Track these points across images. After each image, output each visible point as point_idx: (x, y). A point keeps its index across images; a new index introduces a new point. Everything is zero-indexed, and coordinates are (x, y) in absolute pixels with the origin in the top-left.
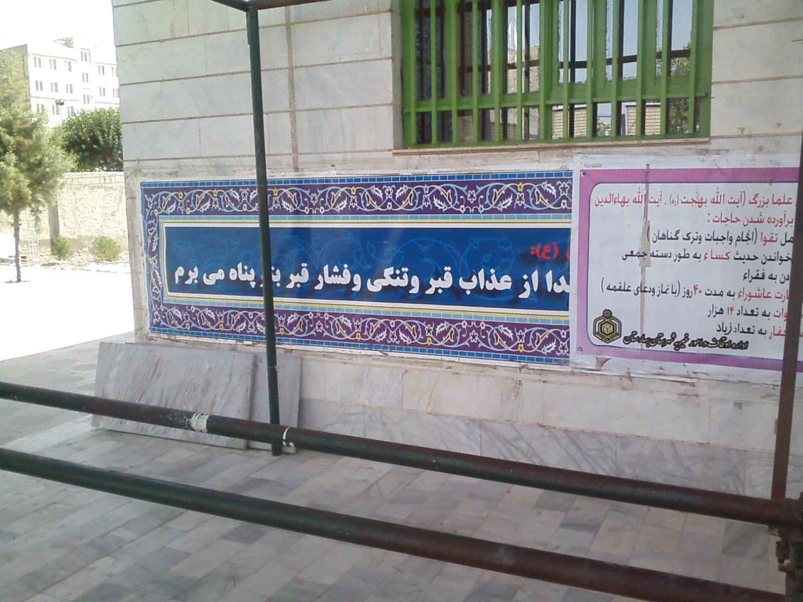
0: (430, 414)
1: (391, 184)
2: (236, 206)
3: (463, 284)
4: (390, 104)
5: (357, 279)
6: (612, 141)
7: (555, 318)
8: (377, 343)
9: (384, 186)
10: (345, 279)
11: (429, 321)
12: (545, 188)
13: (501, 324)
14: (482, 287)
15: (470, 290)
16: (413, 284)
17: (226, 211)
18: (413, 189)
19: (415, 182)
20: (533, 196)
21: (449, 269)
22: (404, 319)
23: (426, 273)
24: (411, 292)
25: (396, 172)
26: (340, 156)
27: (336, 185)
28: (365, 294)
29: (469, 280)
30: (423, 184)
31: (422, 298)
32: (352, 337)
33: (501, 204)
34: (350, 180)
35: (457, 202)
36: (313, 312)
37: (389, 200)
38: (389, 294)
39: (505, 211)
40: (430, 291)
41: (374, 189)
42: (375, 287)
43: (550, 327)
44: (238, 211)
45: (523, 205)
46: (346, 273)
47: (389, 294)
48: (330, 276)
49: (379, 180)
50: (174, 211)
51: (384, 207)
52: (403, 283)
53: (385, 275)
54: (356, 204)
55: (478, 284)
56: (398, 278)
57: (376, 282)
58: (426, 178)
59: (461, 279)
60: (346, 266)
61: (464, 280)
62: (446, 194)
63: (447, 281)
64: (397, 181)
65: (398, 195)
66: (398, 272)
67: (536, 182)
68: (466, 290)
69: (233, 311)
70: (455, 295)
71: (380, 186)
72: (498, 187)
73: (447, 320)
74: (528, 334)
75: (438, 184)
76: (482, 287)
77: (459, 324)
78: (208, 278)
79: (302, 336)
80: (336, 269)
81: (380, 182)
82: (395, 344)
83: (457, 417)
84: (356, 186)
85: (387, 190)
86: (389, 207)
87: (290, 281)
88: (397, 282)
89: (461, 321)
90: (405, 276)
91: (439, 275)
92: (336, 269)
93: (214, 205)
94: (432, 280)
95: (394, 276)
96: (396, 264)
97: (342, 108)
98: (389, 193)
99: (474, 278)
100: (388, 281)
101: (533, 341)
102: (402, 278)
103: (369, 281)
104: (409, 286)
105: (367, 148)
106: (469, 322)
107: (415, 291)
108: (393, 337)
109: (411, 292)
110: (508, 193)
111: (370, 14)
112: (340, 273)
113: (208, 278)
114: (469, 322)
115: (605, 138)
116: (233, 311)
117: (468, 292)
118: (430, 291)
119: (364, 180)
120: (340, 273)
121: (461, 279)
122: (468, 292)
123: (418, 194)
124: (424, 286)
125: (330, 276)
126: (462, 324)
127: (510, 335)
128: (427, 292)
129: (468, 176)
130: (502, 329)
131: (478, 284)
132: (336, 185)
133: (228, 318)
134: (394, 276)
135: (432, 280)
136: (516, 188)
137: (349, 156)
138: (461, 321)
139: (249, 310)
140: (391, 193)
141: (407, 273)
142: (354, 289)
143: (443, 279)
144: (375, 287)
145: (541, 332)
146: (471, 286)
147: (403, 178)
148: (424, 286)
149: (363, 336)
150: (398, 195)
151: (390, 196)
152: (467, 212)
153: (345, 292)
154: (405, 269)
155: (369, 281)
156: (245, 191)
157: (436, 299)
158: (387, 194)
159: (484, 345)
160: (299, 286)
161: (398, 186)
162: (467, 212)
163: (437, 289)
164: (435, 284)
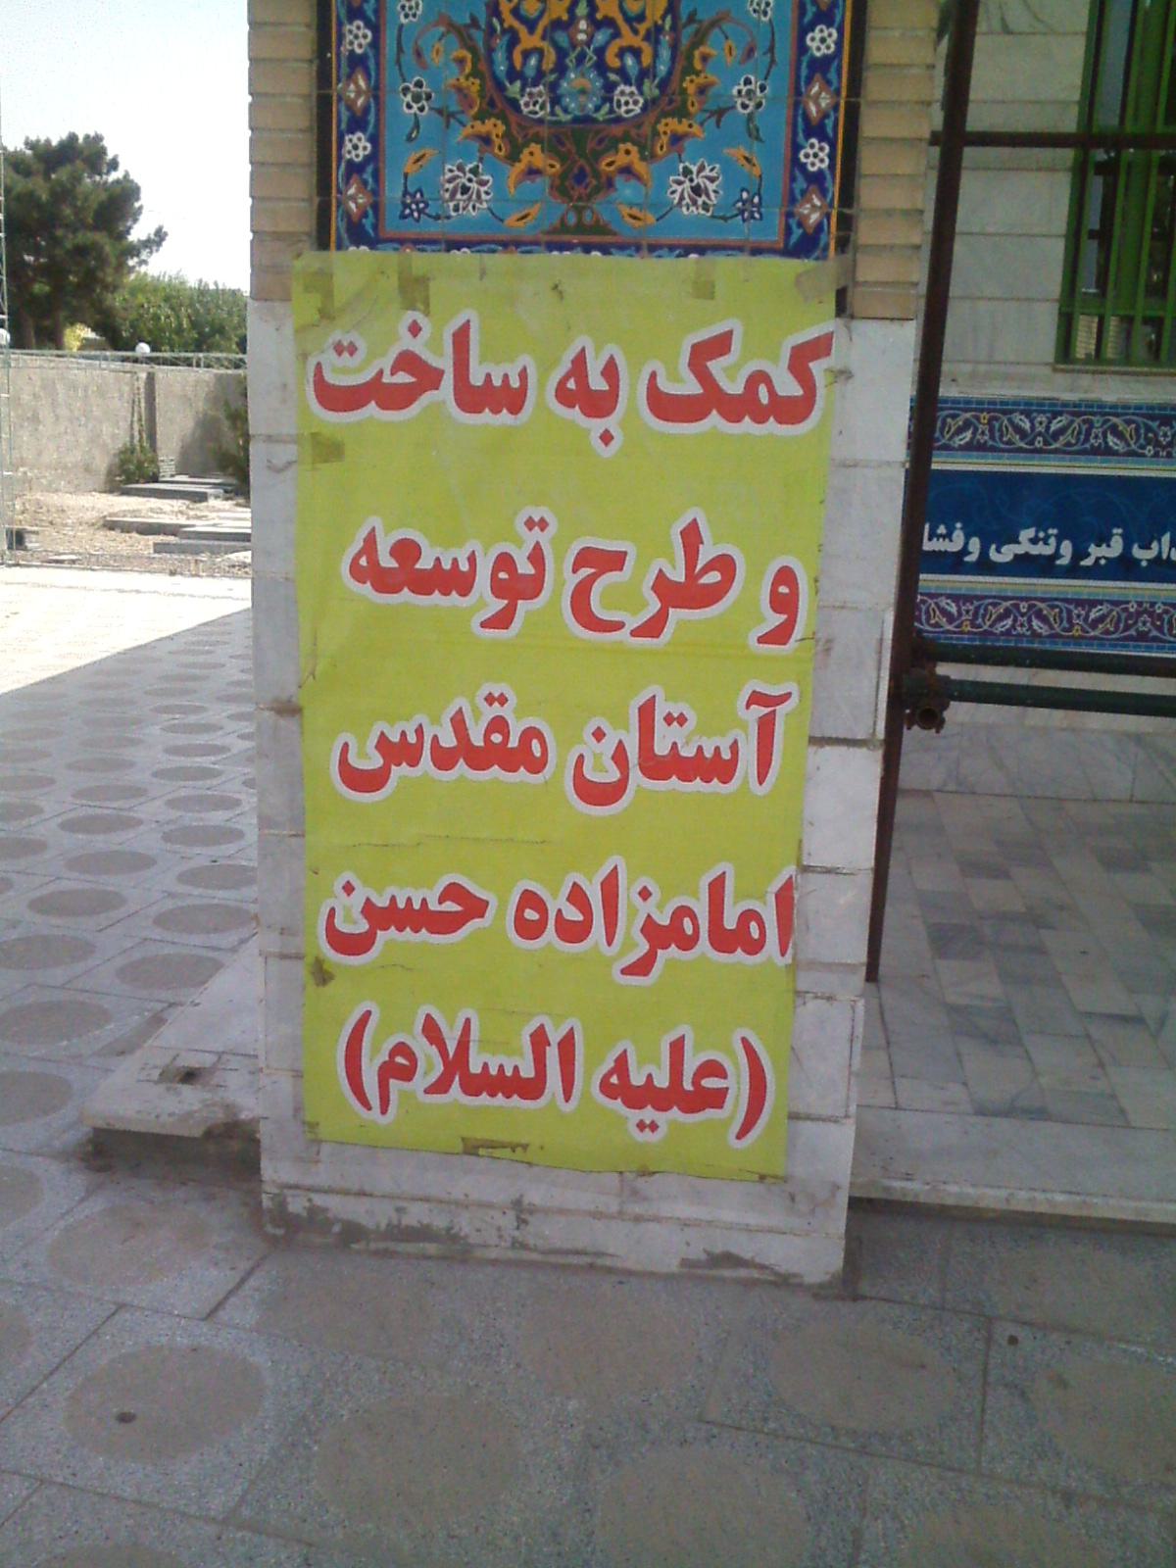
0: (1063, 730)
1: (1044, 412)
2: (1022, 439)
3: (1137, 552)
4: (1053, 300)
5: (975, 544)
6: (1119, 365)
7: (970, 585)
8: (995, 634)
9: (1035, 414)
10: (955, 545)
11: (1079, 603)
12: (1017, 420)
13: (941, 595)
14: (1165, 556)
15: (1148, 561)
16: (971, 548)
17: (1002, 446)
18: (1078, 420)
19: (1076, 410)
20: (1000, 430)
21: (1120, 531)
22: (1043, 600)
23: (1082, 537)
24: (1058, 562)
25: (1055, 395)
26: (967, 368)
27: (959, 409)
28: (985, 566)
29: (1146, 546)
30: (1094, 414)
31: (1074, 571)
32: (956, 627)
33: (957, 439)
34: (980, 402)
35: (1142, 441)
36: (1136, 602)
37: (1040, 434)
38: (1025, 565)
39: (962, 448)
40: (1088, 562)
41: (1018, 418)
42: (1005, 555)
43: (1006, 599)
44: (1028, 447)
45: (986, 442)
46: (959, 536)
47: (1025, 565)
48: (930, 539)
49: (1026, 404)
50: (967, 443)
51: (1031, 443)
52: (1048, 550)
53: (1020, 539)
54: (986, 438)
55: (1160, 553)
56: (1041, 543)
57: (1004, 549)
58: (1100, 407)
59: (1136, 546)
60: (959, 525)
61: (1141, 547)
62: (1128, 430)
63: (1115, 548)
64: (1055, 409)
65: (1053, 427)
66: (1041, 535)
67: (1005, 412)
68: (1141, 560)
69: (991, 601)
70: (1124, 568)
71: (1028, 414)
72: (954, 417)
73: (1107, 601)
74: (977, 609)
75: (1117, 415)
76: (1165, 556)
77: (1124, 606)
78: (998, 551)
79: (1114, 636)
80: (942, 530)
81: (1029, 408)
82: (1023, 635)
83: (1105, 732)
84: (989, 411)
85: (1039, 419)
86: (1039, 443)
87: (1088, 555)
88: (1035, 550)
89: (1128, 602)
90: (1052, 541)
91: (1104, 539)
92: (942, 530)
93: (978, 437)
94: (1093, 545)
95: (1034, 541)
96: (1041, 525)
97: (979, 298)
98: (1041, 423)
99: (1155, 545)
100: (1024, 547)
101: (984, 616)
102: (1046, 543)
103: (993, 547)
104: (1057, 555)
105: (1012, 358)
106: (1140, 604)
107: (1064, 561)
108: (1022, 625)
109: (1058, 562)
110: (967, 425)
111: (1040, 169)
112: (948, 536)
113: (998, 551)
114: (1140, 604)
115: (1111, 362)
116: (991, 601)
117: (1144, 564)
118: (1088, 562)
119: (1002, 403)
120: (948, 536)
121: (1136, 546)
122: (1144, 564)
123: (1084, 427)
124: (1080, 553)
125: (930, 539)
126: (1130, 606)
127: (954, 609)
128: (1083, 563)
129: (1162, 407)
130: (943, 602)
131: (1160, 553)
132: (959, 409)
133: (982, 611)
134: (1034, 541)
135: (1093, 545)
136: (978, 419)
137: (982, 368)
138: (1128, 602)
139: (1022, 599)
140: (1044, 425)
141: (1056, 536)
142: (967, 559)
143: (1109, 546)
144: (1005, 555)
145: (995, 605)
146: (1151, 554)
147: (1065, 404)
148: (1080, 553)
149: (973, 625)
150: (1053, 427)
151: (1040, 429)
152: (1156, 455)
153: (1043, 566)
154: (1053, 531)
155: (993, 547)
156: (1042, 418)
157: (1096, 572)
158: (1037, 425)
159: (1159, 635)
160: (1103, 562)
161: (1055, 415)
162: (1156, 455)
163: (1098, 559)
164: (1095, 551)
